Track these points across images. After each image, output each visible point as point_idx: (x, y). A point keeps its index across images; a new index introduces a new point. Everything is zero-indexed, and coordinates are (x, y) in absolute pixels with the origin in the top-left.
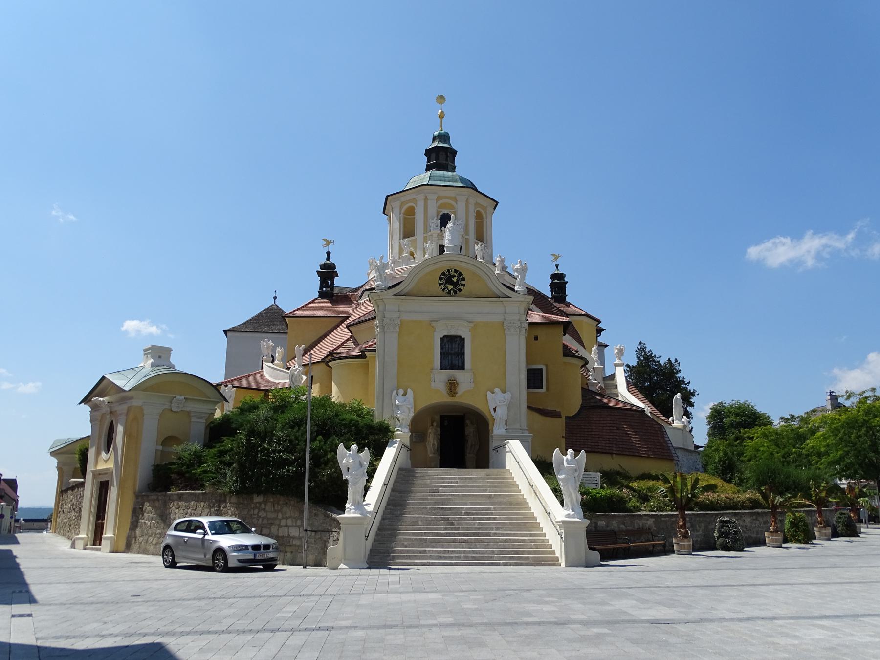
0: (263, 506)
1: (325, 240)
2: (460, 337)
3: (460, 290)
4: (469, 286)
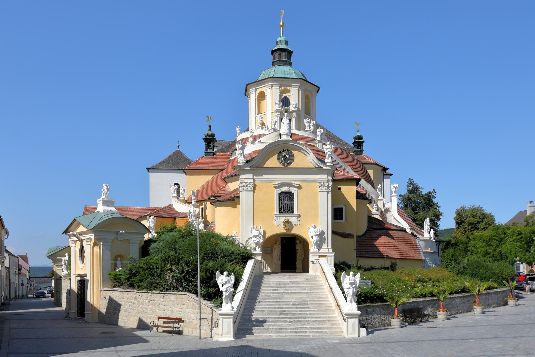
1: (208, 117)
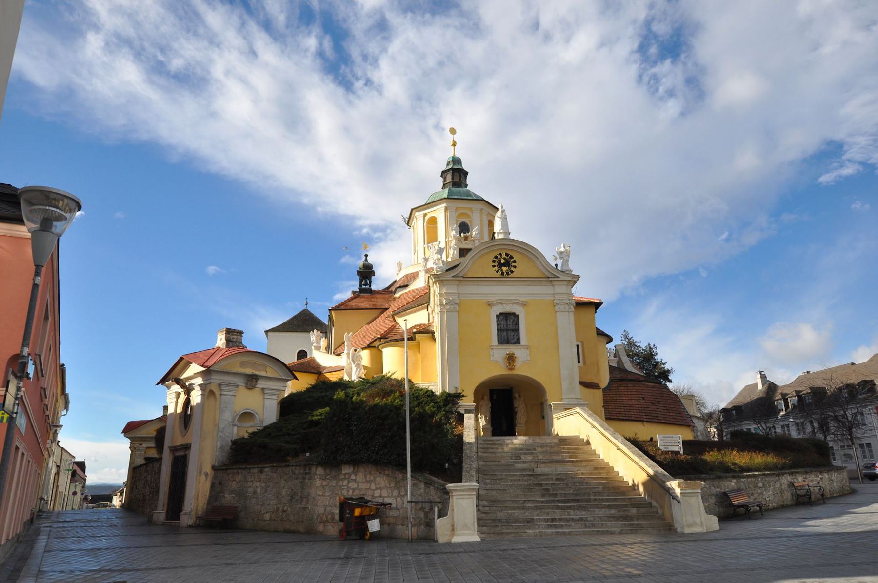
0: (353, 477)
2: (514, 314)
4: (521, 268)
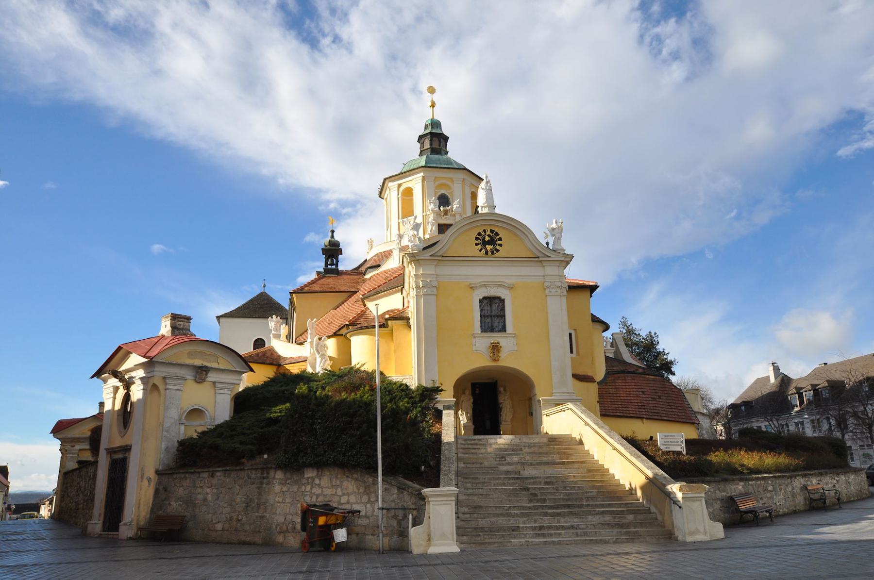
0: (317, 481)
2: (499, 298)
3: (497, 251)
4: (508, 247)
